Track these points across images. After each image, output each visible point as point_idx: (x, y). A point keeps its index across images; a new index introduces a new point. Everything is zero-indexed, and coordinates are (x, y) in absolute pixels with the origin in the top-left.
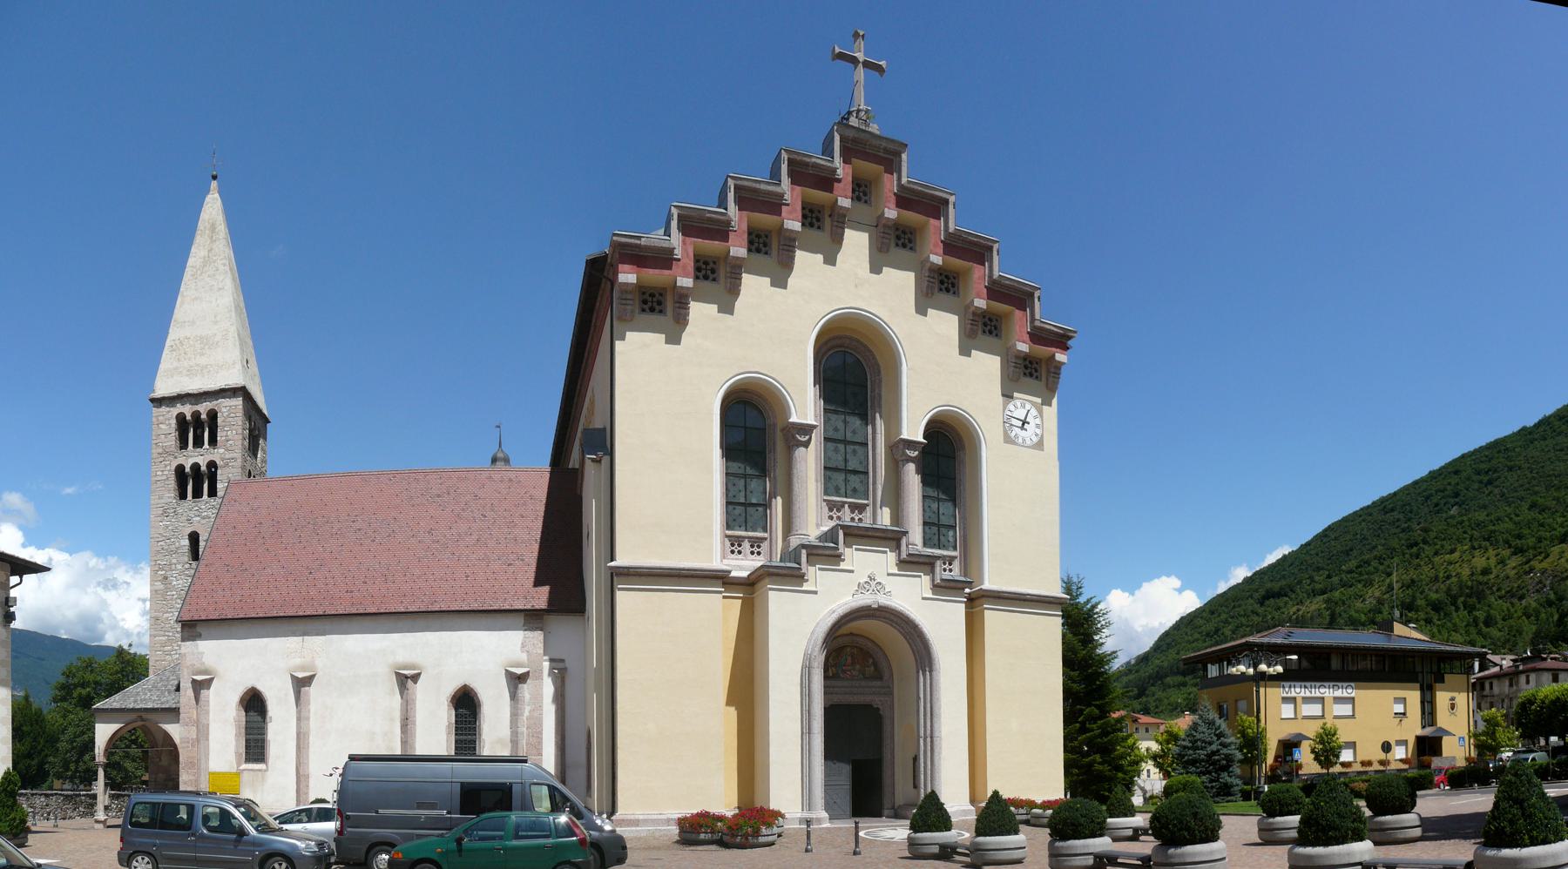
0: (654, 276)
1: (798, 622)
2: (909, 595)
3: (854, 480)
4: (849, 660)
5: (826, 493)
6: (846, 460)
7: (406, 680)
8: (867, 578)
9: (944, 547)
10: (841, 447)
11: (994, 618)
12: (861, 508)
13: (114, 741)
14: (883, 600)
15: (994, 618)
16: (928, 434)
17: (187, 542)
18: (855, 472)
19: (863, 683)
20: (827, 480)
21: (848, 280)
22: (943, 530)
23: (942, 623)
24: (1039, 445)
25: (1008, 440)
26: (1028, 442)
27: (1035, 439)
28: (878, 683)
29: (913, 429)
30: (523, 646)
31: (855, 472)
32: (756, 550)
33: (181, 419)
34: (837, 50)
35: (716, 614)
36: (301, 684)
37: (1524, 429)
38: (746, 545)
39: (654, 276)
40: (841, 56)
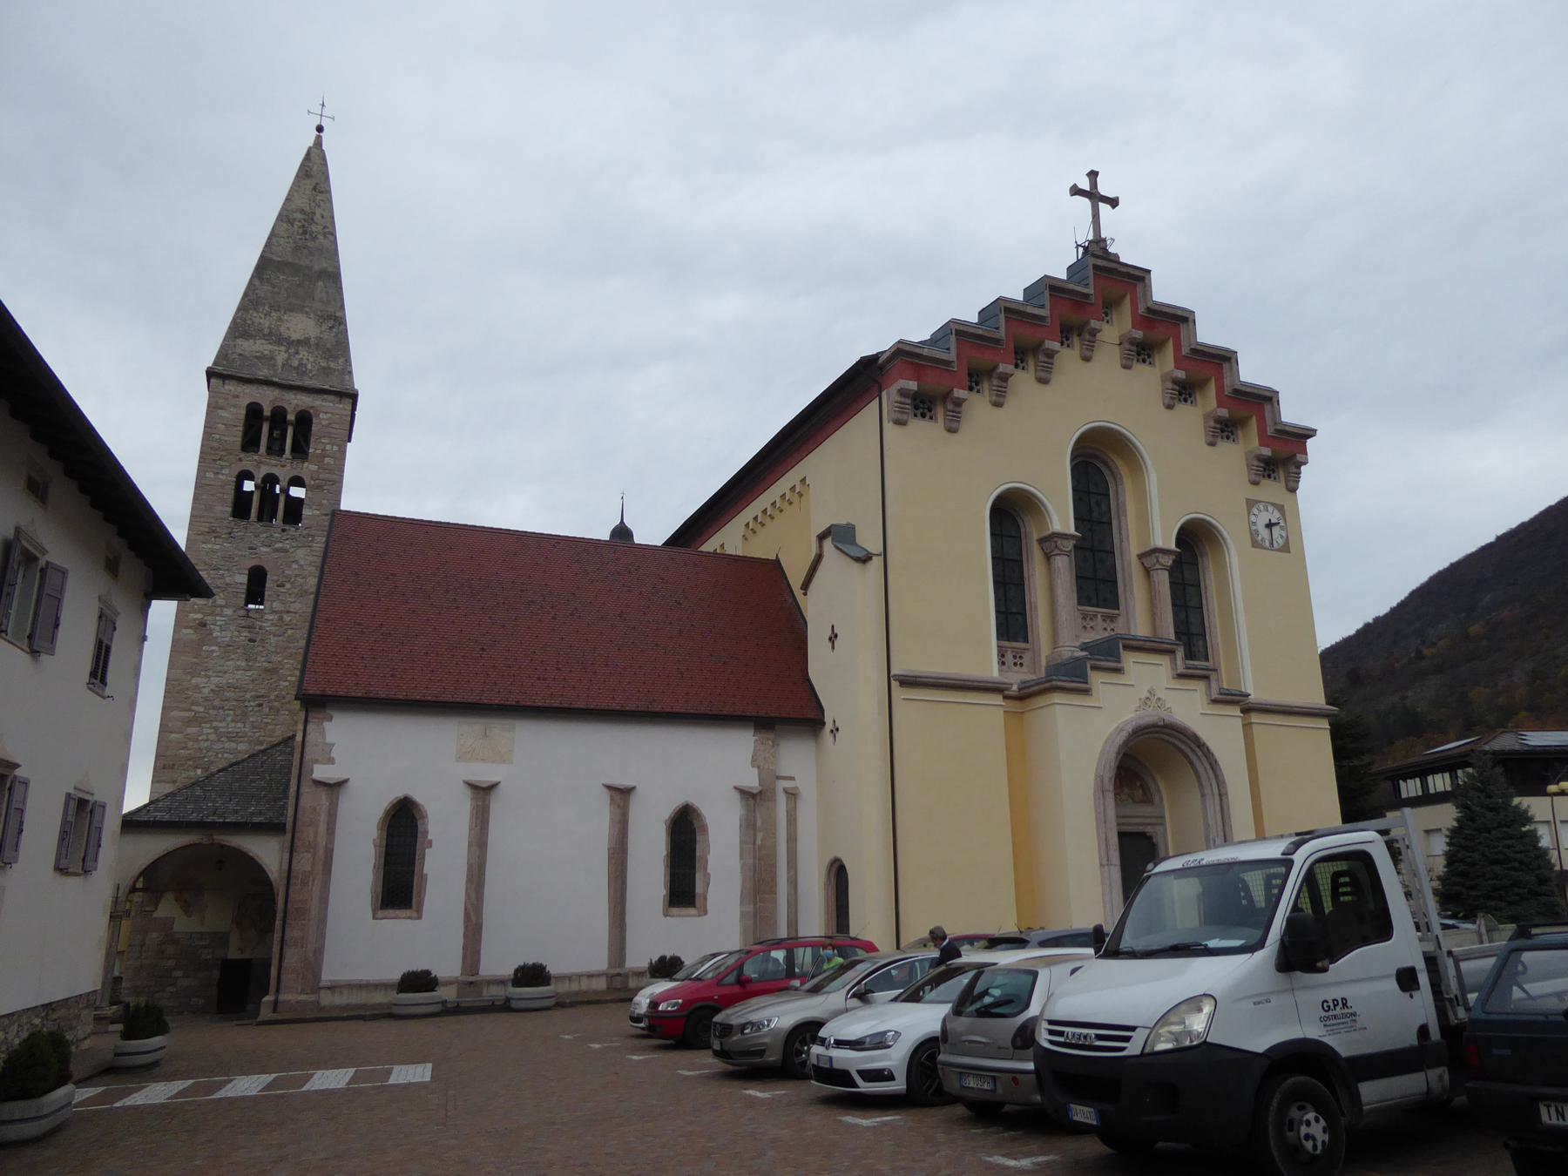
2: (1188, 707)
5: (1080, 603)
6: (1095, 571)
7: (621, 795)
12: (1112, 618)
13: (252, 866)
15: (1255, 718)
16: (1180, 540)
17: (244, 579)
20: (1080, 589)
25: (1256, 544)
27: (1281, 542)
29: (1164, 537)
30: (754, 760)
32: (1018, 661)
33: (254, 412)
35: (990, 713)
36: (482, 792)
37: (1367, 625)
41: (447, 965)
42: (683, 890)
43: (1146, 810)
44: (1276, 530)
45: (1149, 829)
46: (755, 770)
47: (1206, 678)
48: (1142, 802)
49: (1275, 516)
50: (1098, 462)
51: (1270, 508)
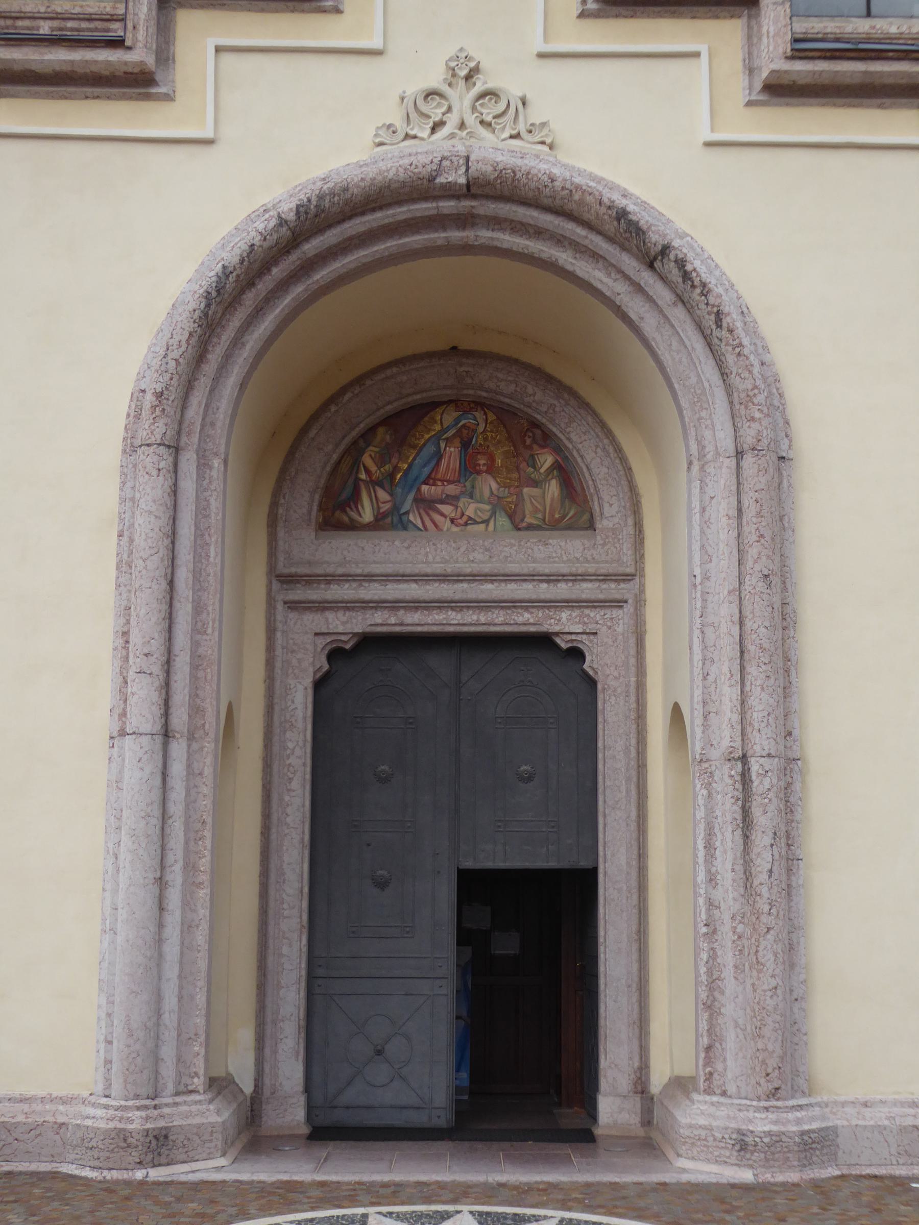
4: (452, 455)
14: (493, 150)
43: (563, 551)
45: (564, 624)
48: (553, 525)
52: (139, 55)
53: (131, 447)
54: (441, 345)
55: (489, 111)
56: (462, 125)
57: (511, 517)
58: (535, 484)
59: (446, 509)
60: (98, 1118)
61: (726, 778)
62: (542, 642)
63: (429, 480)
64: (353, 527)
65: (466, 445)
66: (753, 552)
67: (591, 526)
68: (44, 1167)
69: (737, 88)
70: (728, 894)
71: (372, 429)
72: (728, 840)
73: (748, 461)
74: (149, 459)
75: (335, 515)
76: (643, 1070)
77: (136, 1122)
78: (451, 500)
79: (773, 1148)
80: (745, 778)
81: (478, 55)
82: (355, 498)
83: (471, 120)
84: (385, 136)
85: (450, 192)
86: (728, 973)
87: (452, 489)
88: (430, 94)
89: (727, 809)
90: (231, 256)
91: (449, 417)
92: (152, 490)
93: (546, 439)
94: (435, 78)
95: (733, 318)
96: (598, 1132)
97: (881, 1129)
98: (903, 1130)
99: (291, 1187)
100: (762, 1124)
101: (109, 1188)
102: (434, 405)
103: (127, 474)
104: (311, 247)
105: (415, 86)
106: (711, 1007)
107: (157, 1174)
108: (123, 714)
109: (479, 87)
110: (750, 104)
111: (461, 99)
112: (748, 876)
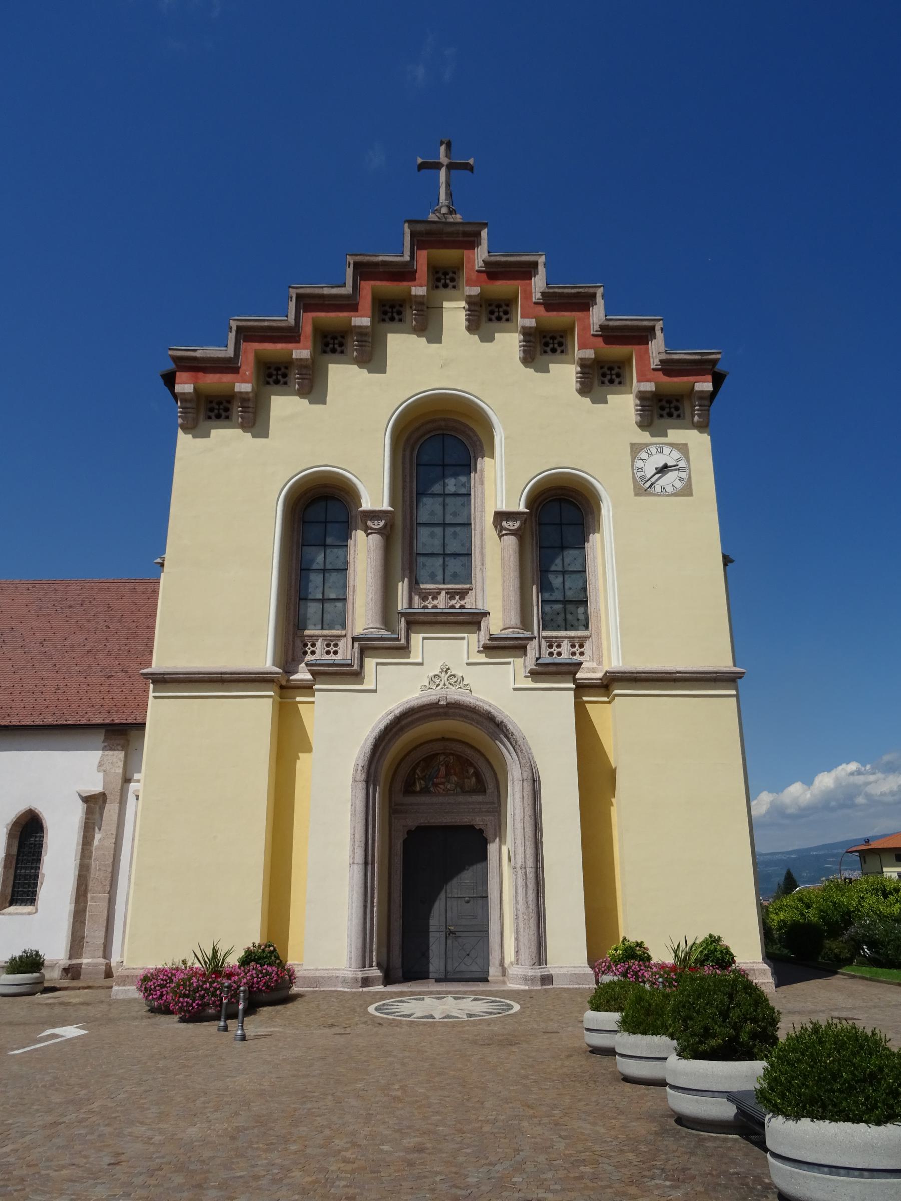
0: (213, 382)
1: (346, 724)
2: (498, 687)
3: (454, 565)
4: (443, 768)
8: (439, 668)
9: (573, 627)
10: (439, 531)
11: (259, 708)
12: (463, 594)
14: (455, 694)
18: (455, 555)
19: (461, 798)
21: (450, 358)
22: (570, 607)
23: (538, 719)
24: (687, 491)
26: (669, 489)
28: (479, 798)
30: (100, 765)
31: (455, 555)
34: (420, 160)
38: (565, 644)
39: (213, 382)
40: (422, 166)
41: (55, 952)
42: (23, 888)
44: (671, 476)
46: (101, 775)
47: (492, 638)
49: (670, 457)
50: (440, 443)
51: (667, 450)
52: (356, 667)
53: (355, 781)
54: (440, 736)
55: (453, 680)
56: (445, 685)
57: (461, 788)
58: (468, 778)
59: (442, 786)
60: (349, 974)
61: (520, 872)
62: (471, 827)
63: (437, 777)
64: (414, 792)
65: (447, 766)
66: (526, 809)
67: (485, 791)
68: (333, 989)
69: (522, 672)
70: (521, 907)
71: (419, 763)
72: (521, 891)
73: (525, 782)
74: (361, 786)
75: (409, 789)
76: (502, 959)
77: (360, 975)
78: (443, 783)
79: (532, 980)
80: (525, 873)
81: (450, 665)
82: (415, 783)
83: (447, 683)
84: (423, 688)
85: (442, 706)
86: (522, 930)
87: (443, 780)
88: (435, 676)
89: (520, 882)
90: (382, 726)
91: (442, 758)
92: (361, 794)
93: (471, 764)
94: (437, 672)
95: (520, 741)
96: (489, 978)
97: (565, 974)
98: (571, 975)
99: (402, 992)
100: (530, 973)
101: (355, 993)
102: (438, 754)
103: (354, 788)
104: (404, 722)
105: (432, 674)
106: (517, 939)
107: (365, 989)
108: (354, 858)
109: (449, 673)
110: (525, 677)
111: (444, 677)
112: (527, 902)
